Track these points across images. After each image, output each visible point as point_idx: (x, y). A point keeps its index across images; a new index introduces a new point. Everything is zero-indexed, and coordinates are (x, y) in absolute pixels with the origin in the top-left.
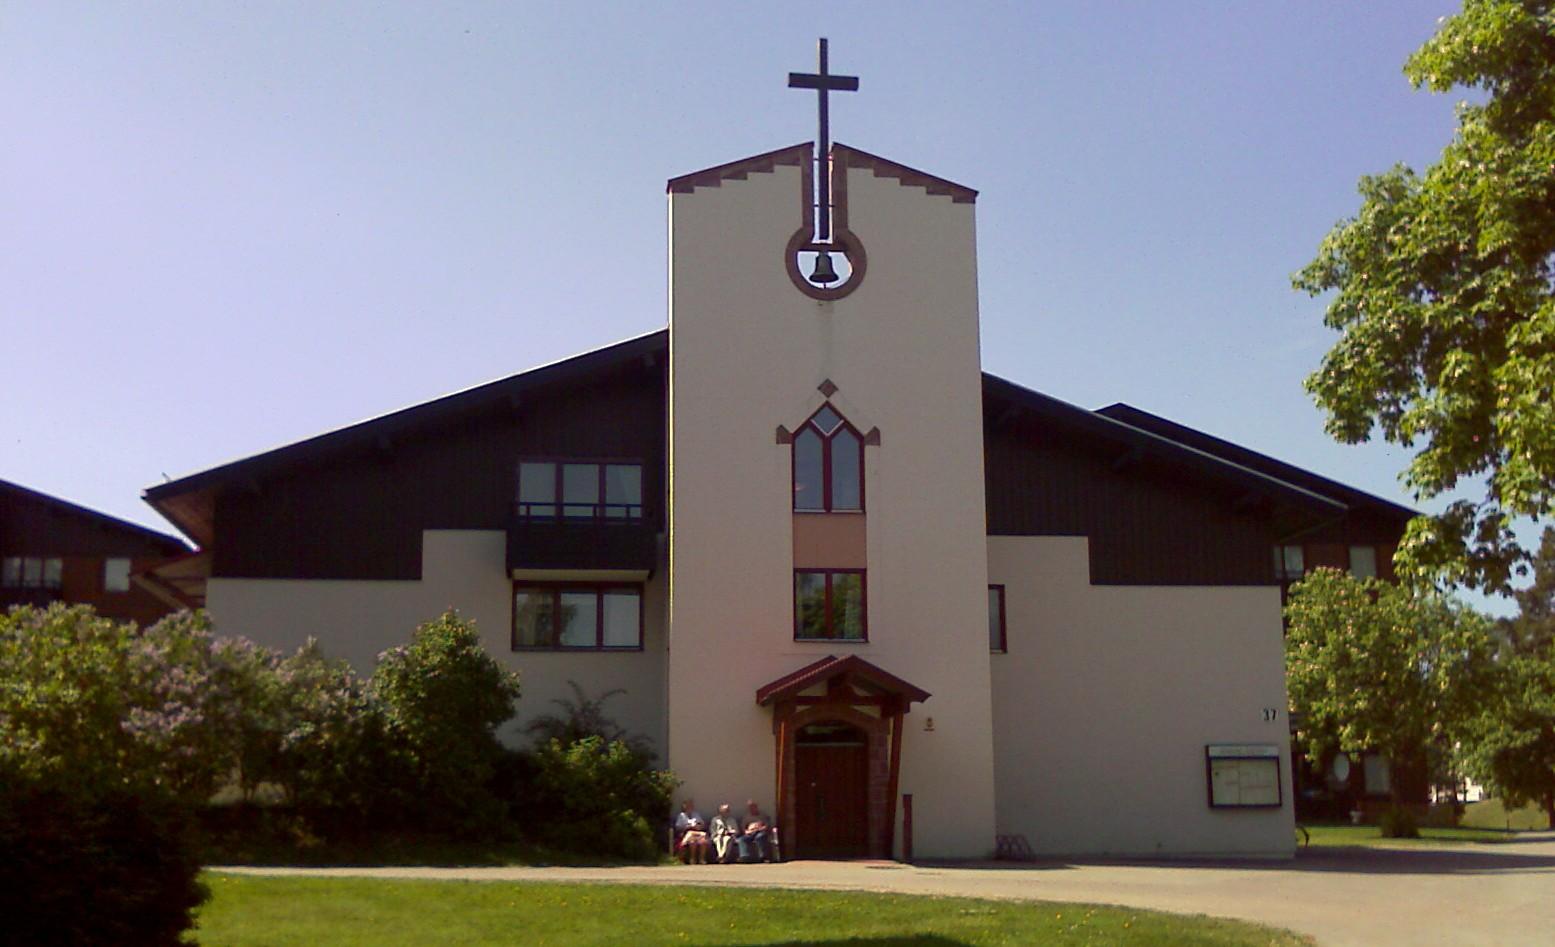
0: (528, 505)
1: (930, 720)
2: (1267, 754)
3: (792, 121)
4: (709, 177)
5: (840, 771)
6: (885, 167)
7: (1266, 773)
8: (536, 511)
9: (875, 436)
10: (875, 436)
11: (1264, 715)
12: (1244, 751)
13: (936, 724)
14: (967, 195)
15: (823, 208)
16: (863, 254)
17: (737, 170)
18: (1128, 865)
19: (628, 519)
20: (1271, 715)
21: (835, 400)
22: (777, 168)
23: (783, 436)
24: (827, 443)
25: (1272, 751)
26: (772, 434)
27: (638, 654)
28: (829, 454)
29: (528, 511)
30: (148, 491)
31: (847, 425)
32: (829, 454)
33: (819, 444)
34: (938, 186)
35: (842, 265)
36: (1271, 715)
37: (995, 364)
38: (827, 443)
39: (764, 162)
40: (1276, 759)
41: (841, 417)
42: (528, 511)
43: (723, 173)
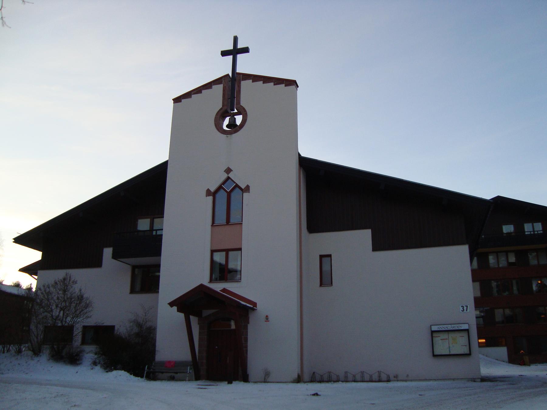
0: (156, 230)
1: (267, 316)
2: (462, 328)
3: (224, 67)
4: (188, 95)
5: (222, 338)
6: (256, 78)
7: (462, 340)
8: (539, 232)
9: (247, 189)
10: (247, 189)
11: (461, 309)
12: (450, 327)
13: (270, 318)
14: (292, 83)
15: (230, 99)
16: (246, 114)
17: (198, 91)
18: (187, 329)
19: (531, 234)
20: (465, 308)
21: (231, 175)
22: (182, 100)
23: (209, 193)
24: (229, 194)
25: (465, 327)
26: (204, 193)
27: (431, 354)
28: (227, 196)
29: (156, 233)
30: (14, 239)
31: (237, 186)
32: (227, 196)
33: (226, 194)
34: (278, 81)
35: (239, 119)
36: (465, 308)
37: (308, 150)
38: (229, 194)
39: (209, 85)
40: (467, 330)
41: (235, 182)
42: (156, 233)
43: (192, 93)
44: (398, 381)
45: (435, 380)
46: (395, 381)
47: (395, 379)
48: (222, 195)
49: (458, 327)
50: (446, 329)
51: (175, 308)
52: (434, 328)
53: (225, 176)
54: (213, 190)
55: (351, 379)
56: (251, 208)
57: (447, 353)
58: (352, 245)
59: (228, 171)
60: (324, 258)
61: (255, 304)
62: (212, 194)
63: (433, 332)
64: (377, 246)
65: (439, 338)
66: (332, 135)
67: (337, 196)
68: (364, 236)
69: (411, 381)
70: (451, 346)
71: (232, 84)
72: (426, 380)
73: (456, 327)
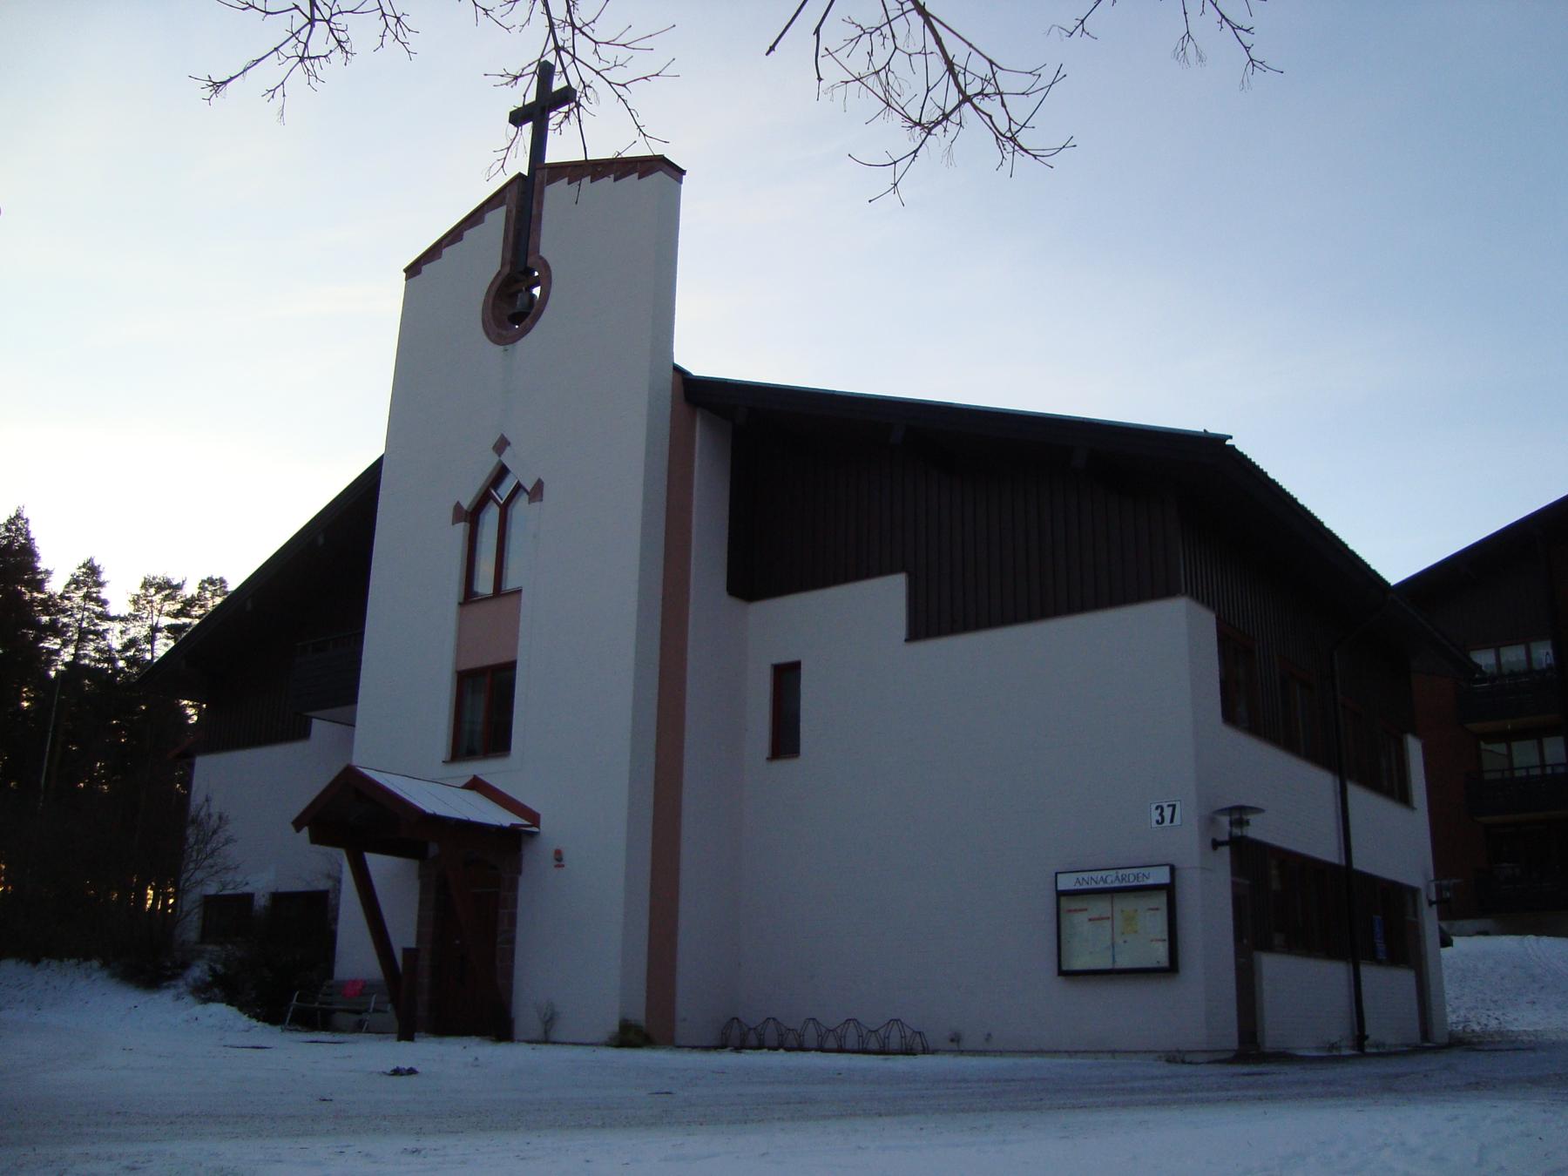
2: (1150, 881)
4: (432, 253)
11: (1156, 815)
12: (1112, 879)
13: (566, 857)
20: (1167, 812)
25: (1161, 876)
36: (1167, 812)
38: (505, 509)
44: (962, 1052)
45: (1070, 1053)
46: (951, 1051)
47: (954, 1046)
48: (491, 516)
49: (1137, 877)
50: (1102, 885)
51: (305, 831)
52: (1067, 882)
53: (490, 463)
54: (466, 504)
55: (815, 1045)
56: (536, 549)
57: (1104, 963)
58: (852, 627)
59: (502, 445)
60: (786, 677)
61: (534, 818)
62: (459, 514)
63: (1060, 894)
64: (922, 625)
65: (1083, 916)
66: (770, 301)
67: (812, 483)
68: (887, 595)
69: (1001, 1053)
70: (1119, 941)
71: (521, 200)
72: (1040, 1052)
73: (1131, 878)
